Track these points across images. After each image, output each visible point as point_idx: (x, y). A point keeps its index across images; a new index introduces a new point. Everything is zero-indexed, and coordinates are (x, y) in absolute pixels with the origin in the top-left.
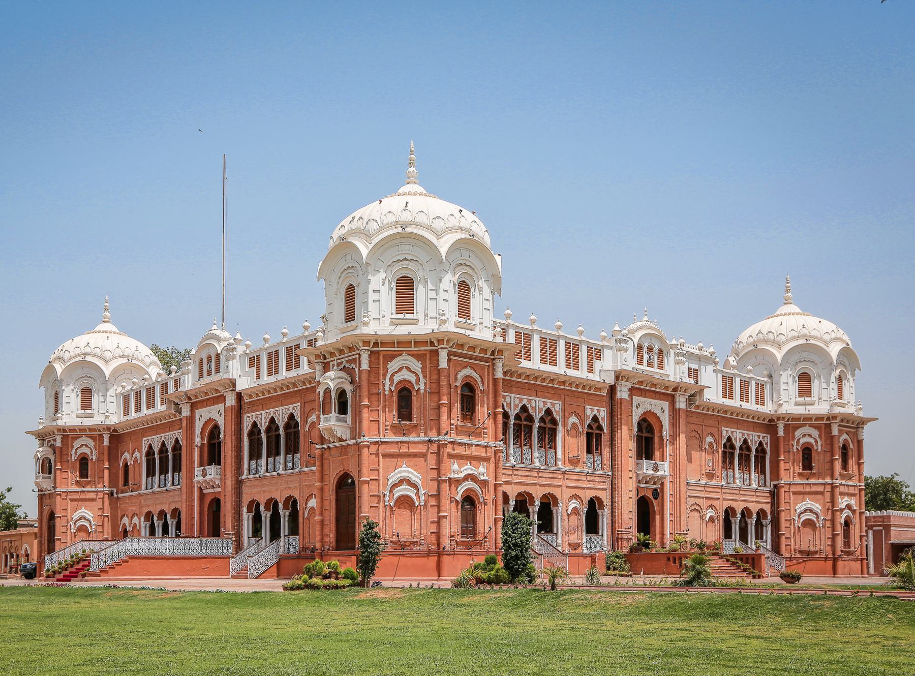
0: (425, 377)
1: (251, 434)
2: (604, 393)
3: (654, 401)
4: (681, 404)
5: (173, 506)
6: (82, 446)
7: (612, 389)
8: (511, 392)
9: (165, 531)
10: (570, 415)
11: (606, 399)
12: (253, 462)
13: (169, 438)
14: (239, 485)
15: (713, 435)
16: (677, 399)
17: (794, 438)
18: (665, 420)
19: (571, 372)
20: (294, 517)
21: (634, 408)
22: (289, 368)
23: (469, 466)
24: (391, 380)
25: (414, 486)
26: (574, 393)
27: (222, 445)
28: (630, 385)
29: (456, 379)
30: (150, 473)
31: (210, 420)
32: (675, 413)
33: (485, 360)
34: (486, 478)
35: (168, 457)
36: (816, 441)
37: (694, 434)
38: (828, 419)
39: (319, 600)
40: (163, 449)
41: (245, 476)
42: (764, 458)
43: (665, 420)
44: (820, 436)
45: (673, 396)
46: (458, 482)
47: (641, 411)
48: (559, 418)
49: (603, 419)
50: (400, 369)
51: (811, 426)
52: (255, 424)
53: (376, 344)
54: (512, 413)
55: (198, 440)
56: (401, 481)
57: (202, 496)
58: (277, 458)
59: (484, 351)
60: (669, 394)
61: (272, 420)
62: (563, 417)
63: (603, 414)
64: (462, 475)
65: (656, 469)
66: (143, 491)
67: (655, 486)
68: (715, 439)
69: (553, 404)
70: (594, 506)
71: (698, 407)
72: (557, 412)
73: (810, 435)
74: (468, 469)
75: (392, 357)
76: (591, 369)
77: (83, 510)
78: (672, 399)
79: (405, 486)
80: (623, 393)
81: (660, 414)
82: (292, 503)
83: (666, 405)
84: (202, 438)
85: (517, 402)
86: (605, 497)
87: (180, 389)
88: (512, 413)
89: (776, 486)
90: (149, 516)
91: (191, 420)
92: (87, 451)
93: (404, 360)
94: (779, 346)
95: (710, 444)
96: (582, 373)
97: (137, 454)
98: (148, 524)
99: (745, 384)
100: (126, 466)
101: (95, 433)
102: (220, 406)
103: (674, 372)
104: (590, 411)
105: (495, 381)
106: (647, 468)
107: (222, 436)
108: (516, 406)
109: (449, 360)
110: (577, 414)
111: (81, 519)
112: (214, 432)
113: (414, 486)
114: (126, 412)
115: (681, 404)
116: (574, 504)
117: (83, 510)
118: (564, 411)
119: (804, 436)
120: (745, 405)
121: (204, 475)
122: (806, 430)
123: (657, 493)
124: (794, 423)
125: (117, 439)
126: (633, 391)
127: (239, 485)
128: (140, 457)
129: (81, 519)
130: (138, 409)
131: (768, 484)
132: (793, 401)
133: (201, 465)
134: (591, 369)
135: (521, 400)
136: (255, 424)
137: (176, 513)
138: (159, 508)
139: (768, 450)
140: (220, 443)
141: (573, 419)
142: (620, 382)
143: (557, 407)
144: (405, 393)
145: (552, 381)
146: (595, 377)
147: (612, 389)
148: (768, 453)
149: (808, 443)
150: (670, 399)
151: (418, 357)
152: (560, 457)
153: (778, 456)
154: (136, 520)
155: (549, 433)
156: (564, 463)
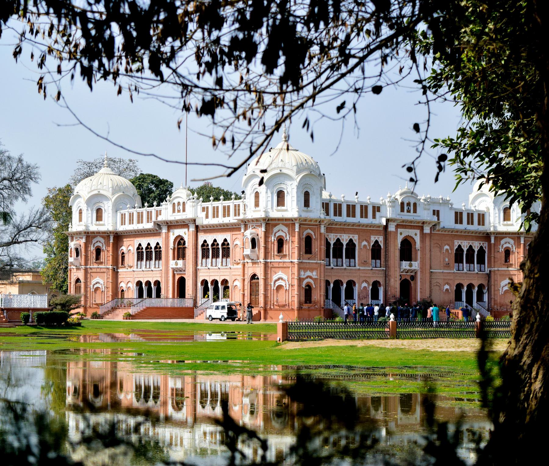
0: (289, 234)
1: (203, 245)
3: (410, 230)
4: (427, 230)
5: (155, 279)
6: (97, 242)
7: (386, 227)
8: (332, 233)
9: (150, 295)
10: (363, 241)
11: (383, 232)
12: (204, 260)
13: (153, 242)
14: (196, 271)
15: (448, 245)
16: (425, 228)
17: (500, 244)
18: (417, 239)
20: (226, 288)
21: (399, 235)
22: (224, 216)
24: (275, 235)
26: (364, 231)
27: (187, 250)
28: (395, 224)
29: (303, 235)
31: (179, 236)
32: (423, 235)
33: (316, 225)
34: (316, 277)
36: (512, 246)
37: (436, 245)
40: (148, 246)
41: (199, 267)
43: (417, 239)
44: (515, 243)
46: (304, 279)
47: (403, 236)
48: (356, 243)
49: (381, 242)
50: (279, 231)
51: (510, 237)
52: (205, 241)
53: (269, 220)
54: (332, 243)
55: (171, 245)
56: (279, 279)
57: (174, 275)
59: (316, 221)
60: (420, 226)
61: (215, 241)
62: (359, 242)
63: (381, 239)
64: (305, 277)
65: (411, 265)
66: (135, 269)
67: (412, 274)
68: (450, 247)
69: (353, 237)
70: (376, 285)
71: (439, 230)
72: (356, 240)
73: (509, 243)
74: (308, 273)
75: (275, 225)
76: (374, 217)
77: (98, 278)
78: (422, 229)
79: (280, 281)
80: (392, 228)
81: (414, 237)
83: (418, 232)
84: (174, 244)
85: (335, 237)
86: (382, 281)
88: (332, 243)
89: (490, 271)
90: (139, 284)
91: (167, 238)
92: (100, 245)
93: (281, 227)
95: (447, 250)
96: (369, 220)
97: (130, 248)
100: (123, 253)
101: (106, 235)
102: (186, 230)
103: (424, 214)
104: (373, 239)
105: (320, 233)
106: (405, 265)
108: (334, 239)
109: (300, 227)
110: (366, 241)
111: (97, 283)
112: (180, 241)
113: (285, 280)
114: (123, 223)
115: (427, 230)
116: (364, 284)
117: (98, 278)
118: (359, 239)
119: (506, 243)
120: (470, 227)
121: (177, 264)
122: (508, 240)
123: (413, 278)
124: (500, 236)
125: (118, 238)
126: (397, 226)
127: (196, 271)
128: (133, 249)
129: (97, 283)
131: (486, 269)
133: (174, 259)
134: (374, 217)
135: (336, 236)
136: (205, 241)
137: (157, 283)
138: (146, 280)
139: (486, 250)
141: (365, 243)
142: (390, 223)
143: (356, 238)
145: (353, 225)
146: (376, 222)
147: (386, 227)
148: (487, 252)
149: (508, 247)
150: (420, 228)
151: (286, 225)
153: (491, 254)
154: (130, 285)
155: (351, 254)
156: (359, 265)
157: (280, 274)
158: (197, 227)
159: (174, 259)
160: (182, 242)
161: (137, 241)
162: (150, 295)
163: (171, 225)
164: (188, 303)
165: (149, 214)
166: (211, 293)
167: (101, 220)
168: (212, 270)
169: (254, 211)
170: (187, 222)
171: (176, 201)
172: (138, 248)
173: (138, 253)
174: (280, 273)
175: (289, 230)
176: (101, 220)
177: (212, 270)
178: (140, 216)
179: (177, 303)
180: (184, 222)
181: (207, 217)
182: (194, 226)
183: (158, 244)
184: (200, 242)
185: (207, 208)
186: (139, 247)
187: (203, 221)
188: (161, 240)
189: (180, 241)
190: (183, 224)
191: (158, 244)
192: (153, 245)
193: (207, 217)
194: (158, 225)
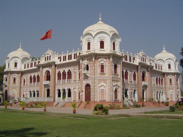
1: (58, 74)
2: (136, 67)
9: (34, 96)
19: (126, 61)
23: (116, 83)
25: (105, 87)
30: (31, 82)
35: (36, 78)
38: (109, 55)
39: (40, 112)
40: (34, 77)
42: (135, 76)
45: (148, 68)
58: (65, 80)
79: (102, 87)
82: (69, 90)
87: (39, 64)
94: (94, 31)
98: (30, 93)
99: (130, 58)
107: (50, 74)
112: (48, 72)
113: (105, 87)
114: (25, 68)
130: (28, 67)
132: (98, 50)
140: (50, 76)
144: (102, 66)
152: (128, 80)
157: (14, 90)
158: (56, 66)
159: (45, 81)
160: (48, 73)
161: (29, 75)
162: (34, 96)
163: (44, 66)
164: (51, 99)
165: (35, 63)
166: (33, 95)
167: (104, 48)
168: (62, 85)
169: (14, 69)
170: (51, 64)
171: (46, 56)
172: (30, 77)
173: (30, 79)
174: (102, 83)
175: (107, 61)
176: (104, 48)
177: (62, 85)
178: (32, 64)
179: (46, 99)
180: (50, 64)
181: (60, 61)
182: (54, 66)
183: (38, 75)
184: (57, 72)
185: (61, 57)
186: (31, 77)
187: (58, 62)
188: (39, 73)
189: (48, 72)
190: (49, 65)
191: (38, 75)
192: (66, 72)
193: (60, 61)
194: (39, 67)
